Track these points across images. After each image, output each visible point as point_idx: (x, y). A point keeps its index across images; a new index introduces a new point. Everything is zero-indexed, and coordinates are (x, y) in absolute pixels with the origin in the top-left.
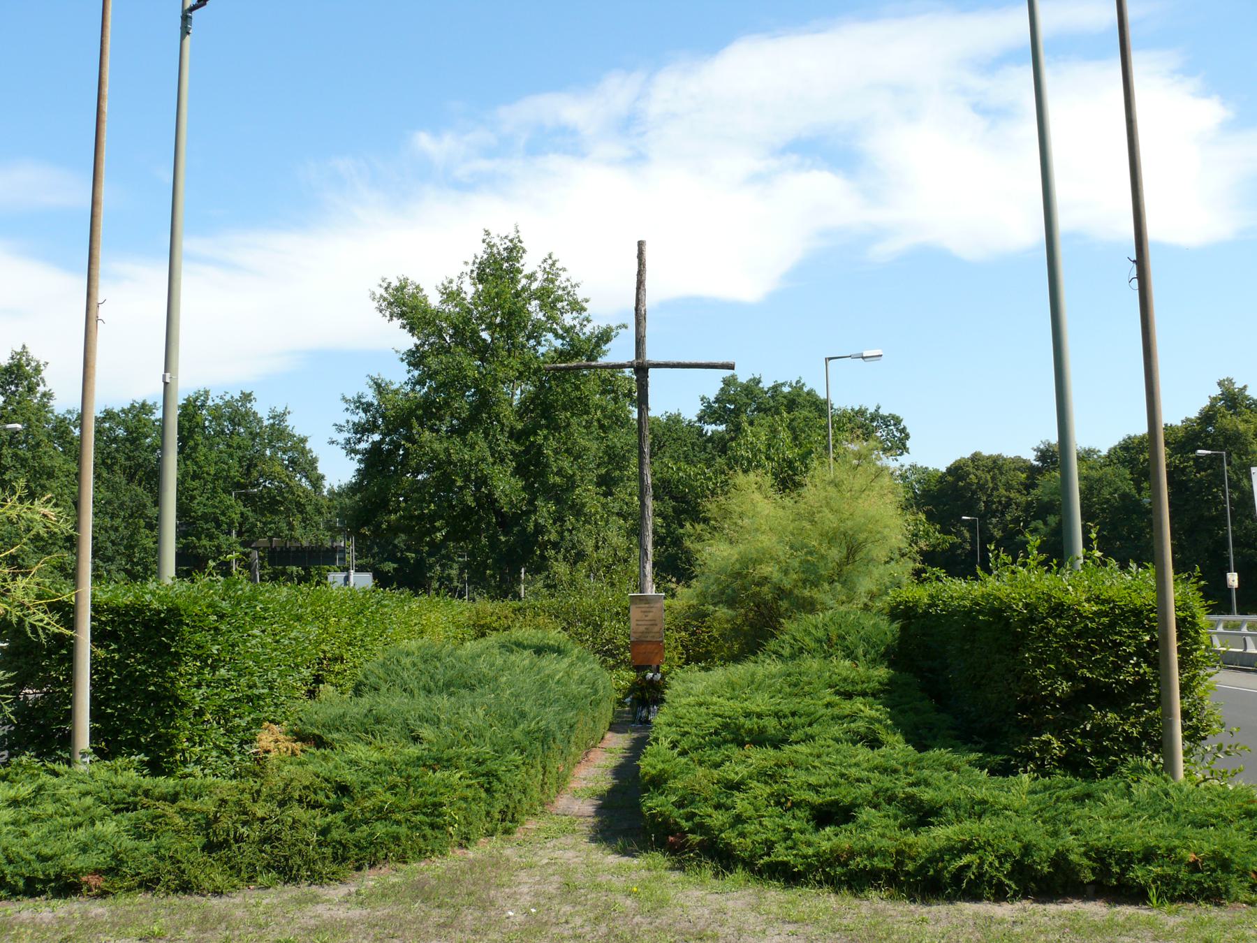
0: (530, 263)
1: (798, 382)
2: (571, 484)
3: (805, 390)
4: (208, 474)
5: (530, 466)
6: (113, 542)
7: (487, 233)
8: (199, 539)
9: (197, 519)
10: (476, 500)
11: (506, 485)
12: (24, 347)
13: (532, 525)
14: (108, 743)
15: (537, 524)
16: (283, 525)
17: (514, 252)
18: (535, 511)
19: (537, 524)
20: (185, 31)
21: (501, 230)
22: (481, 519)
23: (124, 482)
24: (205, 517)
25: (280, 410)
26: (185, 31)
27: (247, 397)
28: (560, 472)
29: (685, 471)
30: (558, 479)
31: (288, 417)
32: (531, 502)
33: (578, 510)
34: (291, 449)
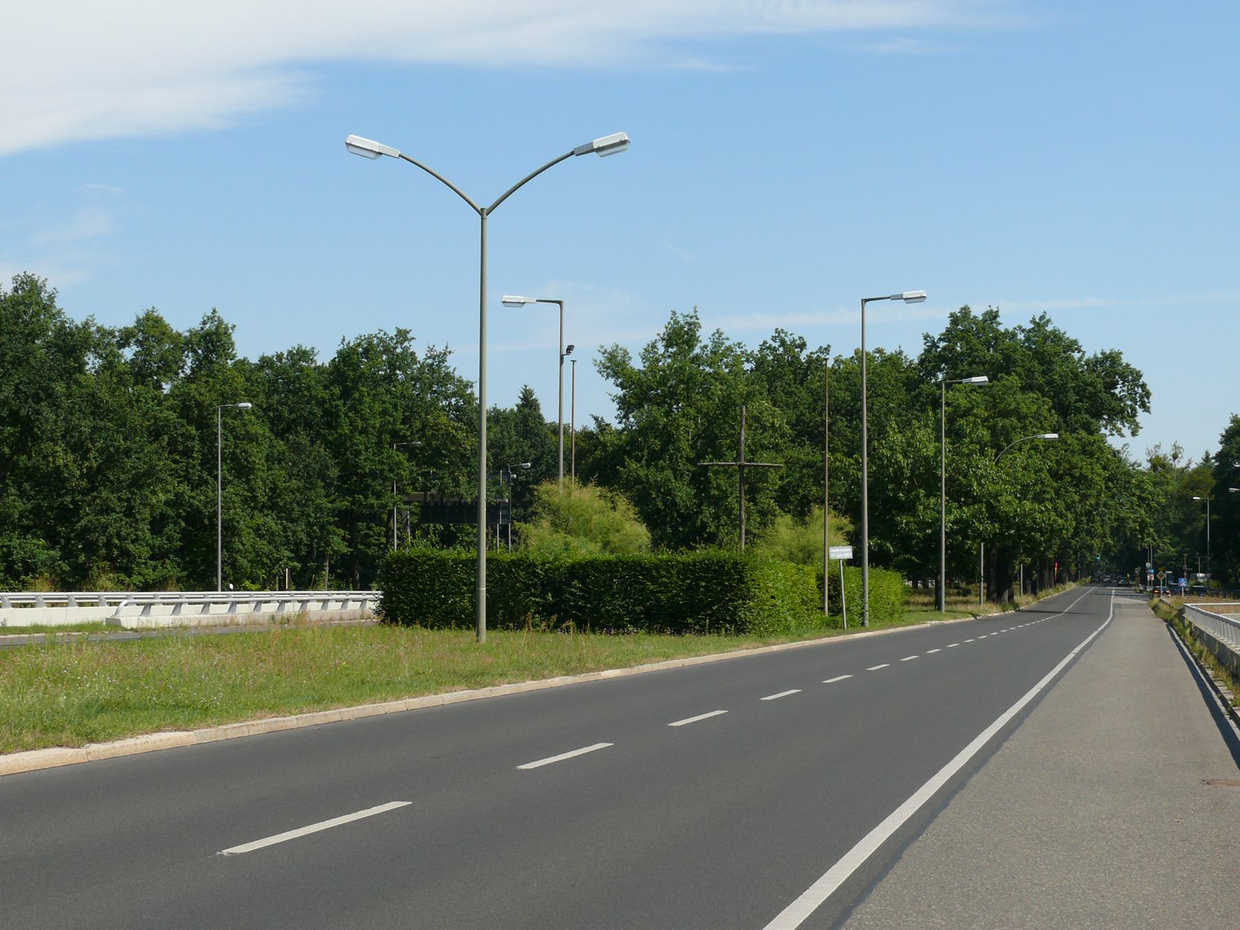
0: (705, 336)
1: (1042, 318)
2: (724, 496)
3: (1049, 328)
4: (374, 427)
5: (699, 480)
6: (298, 503)
7: (674, 313)
8: (366, 497)
9: (365, 475)
10: (665, 504)
11: (683, 493)
12: (214, 311)
13: (699, 523)
14: (491, 625)
15: (702, 522)
16: (448, 480)
17: (693, 326)
18: (701, 512)
19: (702, 522)
20: (562, 363)
21: (684, 311)
22: (667, 515)
23: (308, 443)
24: (373, 475)
25: (439, 349)
26: (562, 363)
27: (403, 335)
28: (718, 487)
29: (841, 461)
30: (716, 492)
31: (449, 358)
32: (699, 506)
33: (728, 512)
34: (454, 394)
